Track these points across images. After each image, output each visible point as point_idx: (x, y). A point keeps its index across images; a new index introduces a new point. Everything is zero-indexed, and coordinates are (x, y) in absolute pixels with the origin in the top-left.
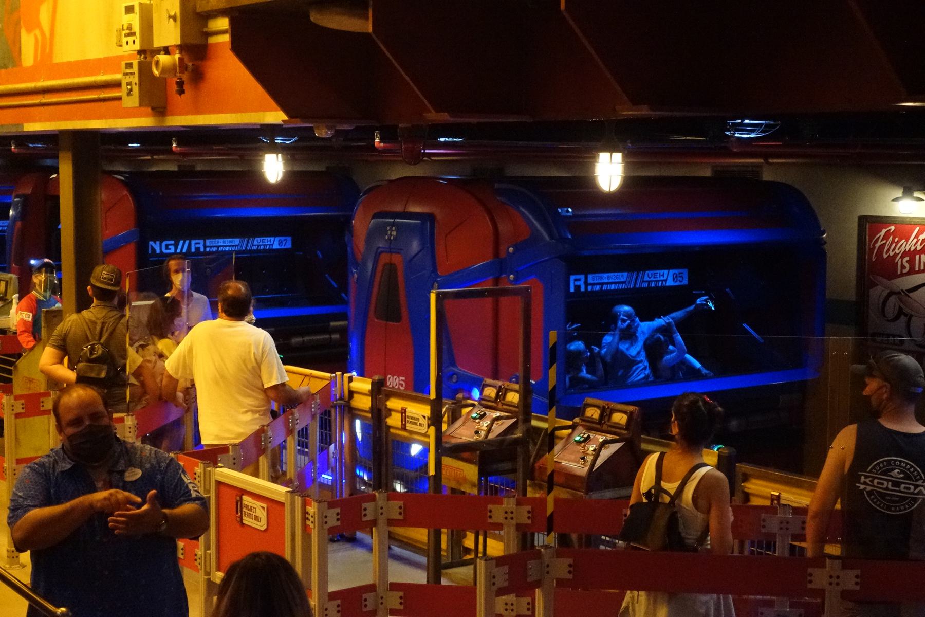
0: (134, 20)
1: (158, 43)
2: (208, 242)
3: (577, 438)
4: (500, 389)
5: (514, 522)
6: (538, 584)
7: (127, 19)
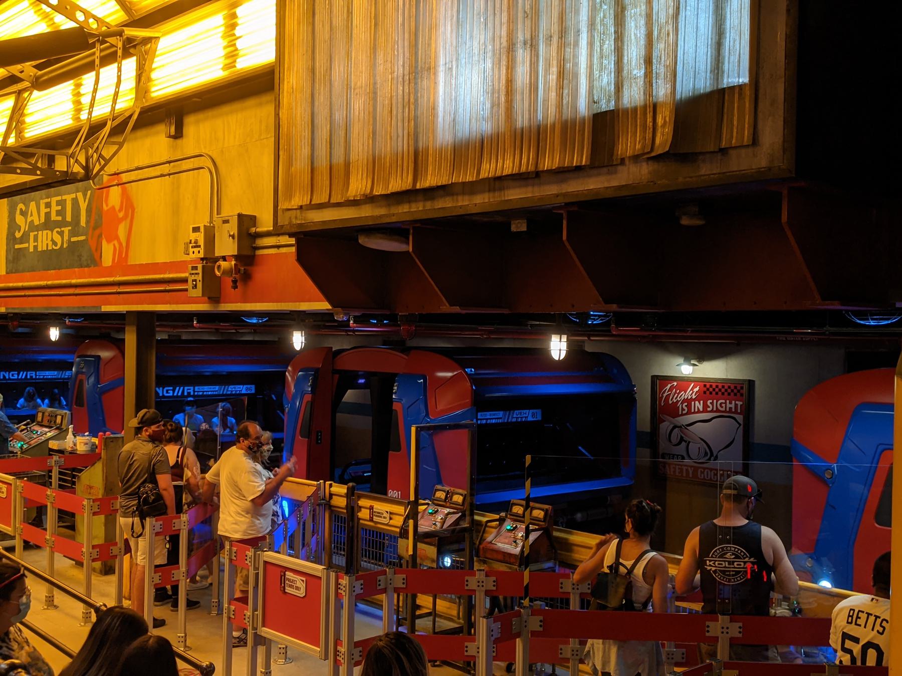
0: (200, 237)
1: (218, 253)
2: (197, 388)
3: (509, 528)
4: (448, 493)
5: (484, 589)
6: (518, 635)
7: (193, 236)
